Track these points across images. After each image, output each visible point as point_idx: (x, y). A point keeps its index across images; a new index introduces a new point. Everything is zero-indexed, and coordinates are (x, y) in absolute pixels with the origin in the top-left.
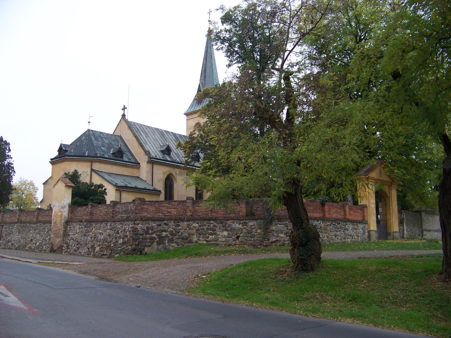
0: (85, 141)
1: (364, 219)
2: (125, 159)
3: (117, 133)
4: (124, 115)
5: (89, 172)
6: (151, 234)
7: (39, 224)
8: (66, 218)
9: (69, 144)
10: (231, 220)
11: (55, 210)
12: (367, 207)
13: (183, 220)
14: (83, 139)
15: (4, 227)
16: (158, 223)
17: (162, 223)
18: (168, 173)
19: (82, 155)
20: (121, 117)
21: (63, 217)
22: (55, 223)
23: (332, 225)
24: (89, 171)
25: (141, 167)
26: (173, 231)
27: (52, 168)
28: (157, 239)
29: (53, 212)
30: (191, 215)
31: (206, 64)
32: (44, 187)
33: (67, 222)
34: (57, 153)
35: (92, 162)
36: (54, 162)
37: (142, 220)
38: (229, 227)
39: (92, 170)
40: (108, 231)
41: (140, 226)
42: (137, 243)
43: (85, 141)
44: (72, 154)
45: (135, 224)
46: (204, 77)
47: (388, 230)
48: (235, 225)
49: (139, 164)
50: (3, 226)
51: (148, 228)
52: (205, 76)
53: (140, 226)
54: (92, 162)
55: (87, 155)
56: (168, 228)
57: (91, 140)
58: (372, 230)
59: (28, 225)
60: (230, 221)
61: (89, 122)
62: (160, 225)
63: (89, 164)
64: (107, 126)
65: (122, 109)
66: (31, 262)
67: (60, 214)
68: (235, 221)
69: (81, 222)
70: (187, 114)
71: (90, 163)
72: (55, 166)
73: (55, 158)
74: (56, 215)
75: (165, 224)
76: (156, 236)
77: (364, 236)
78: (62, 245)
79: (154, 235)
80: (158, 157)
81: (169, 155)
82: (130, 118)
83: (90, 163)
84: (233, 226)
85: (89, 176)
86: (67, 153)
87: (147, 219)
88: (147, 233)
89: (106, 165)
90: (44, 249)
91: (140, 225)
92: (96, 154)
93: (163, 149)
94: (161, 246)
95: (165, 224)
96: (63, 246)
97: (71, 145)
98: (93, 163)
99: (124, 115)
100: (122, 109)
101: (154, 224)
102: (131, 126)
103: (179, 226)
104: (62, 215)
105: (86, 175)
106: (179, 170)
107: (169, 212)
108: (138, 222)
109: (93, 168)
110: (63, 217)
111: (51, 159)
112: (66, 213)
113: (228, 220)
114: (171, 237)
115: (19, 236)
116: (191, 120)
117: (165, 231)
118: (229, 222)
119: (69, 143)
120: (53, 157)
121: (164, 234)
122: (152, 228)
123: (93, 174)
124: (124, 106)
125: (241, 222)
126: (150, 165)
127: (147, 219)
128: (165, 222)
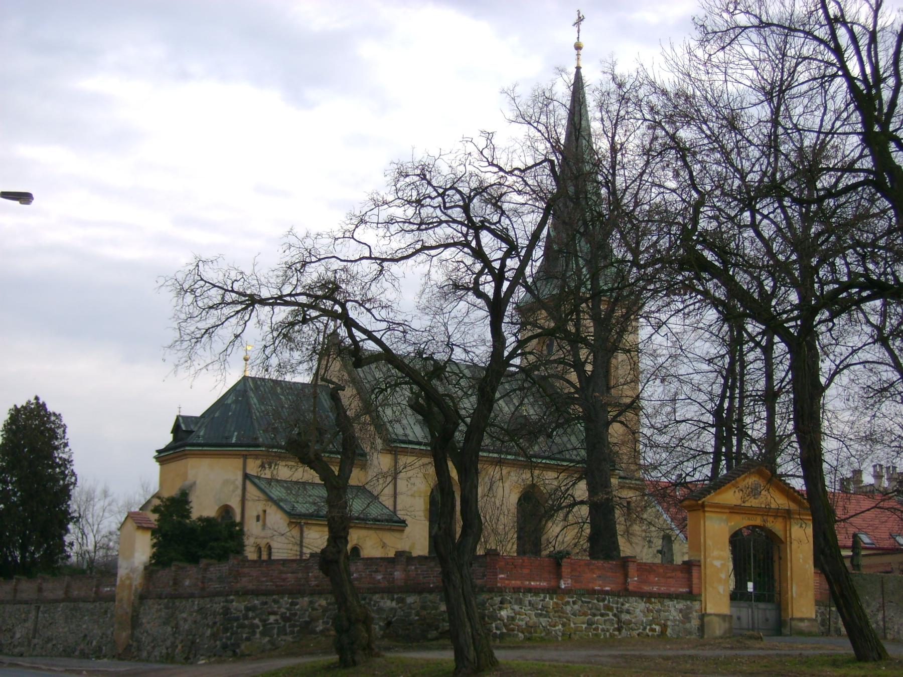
0: (233, 406)
1: (691, 592)
7: (97, 604)
8: (139, 590)
9: (198, 414)
10: (378, 593)
11: (122, 572)
12: (700, 566)
13: (302, 593)
14: (229, 401)
15: (41, 609)
16: (264, 599)
17: (269, 599)
19: (224, 442)
21: (134, 587)
22: (121, 600)
23: (580, 603)
29: (118, 579)
30: (317, 586)
33: (143, 597)
34: (169, 438)
35: (245, 457)
37: (237, 593)
38: (374, 606)
39: (246, 476)
41: (238, 606)
43: (233, 406)
44: (201, 441)
45: (227, 601)
47: (783, 614)
48: (385, 603)
51: (248, 609)
53: (238, 606)
55: (234, 441)
56: (279, 608)
57: (248, 404)
58: (710, 615)
60: (377, 596)
62: (266, 603)
63: (239, 462)
67: (128, 582)
68: (385, 595)
69: (160, 598)
71: (241, 461)
72: (173, 466)
73: (167, 449)
77: (688, 625)
79: (257, 621)
80: (411, 437)
83: (241, 461)
84: (382, 604)
85: (239, 492)
86: (192, 439)
87: (246, 593)
88: (246, 617)
90: (104, 651)
91: (234, 603)
92: (257, 438)
94: (267, 639)
97: (203, 416)
101: (256, 602)
103: (297, 604)
104: (131, 585)
105: (231, 488)
107: (284, 580)
108: (232, 597)
110: (134, 587)
111: (159, 451)
112: (138, 580)
113: (376, 593)
114: (282, 623)
115: (66, 629)
117: (274, 613)
118: (376, 597)
119: (198, 413)
120: (162, 447)
121: (272, 618)
122: (253, 609)
125: (396, 596)
127: (246, 593)
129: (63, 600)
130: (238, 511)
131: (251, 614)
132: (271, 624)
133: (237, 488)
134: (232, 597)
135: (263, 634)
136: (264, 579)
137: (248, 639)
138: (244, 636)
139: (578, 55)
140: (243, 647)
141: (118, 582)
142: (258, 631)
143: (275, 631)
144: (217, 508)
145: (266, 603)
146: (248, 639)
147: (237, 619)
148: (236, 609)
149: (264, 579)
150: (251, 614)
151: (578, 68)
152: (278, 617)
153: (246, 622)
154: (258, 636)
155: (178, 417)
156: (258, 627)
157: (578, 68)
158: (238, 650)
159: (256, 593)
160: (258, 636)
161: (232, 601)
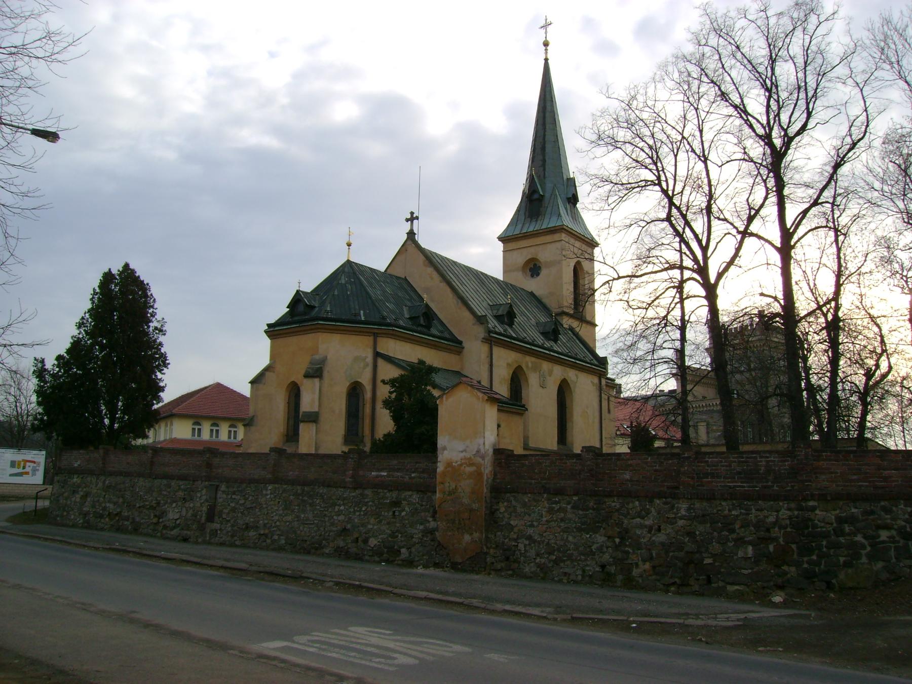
2: (434, 331)
3: (398, 272)
4: (411, 234)
5: (370, 359)
6: (849, 534)
18: (515, 366)
20: (405, 237)
24: (369, 355)
25: (465, 350)
26: (905, 526)
27: (271, 347)
28: (869, 548)
31: (544, 135)
32: (252, 388)
33: (497, 491)
34: (281, 310)
35: (376, 335)
36: (274, 331)
39: (377, 355)
40: (681, 523)
41: (824, 516)
42: (814, 557)
45: (800, 509)
46: (541, 163)
49: (460, 343)
50: (218, 486)
51: (840, 520)
52: (544, 161)
54: (376, 335)
59: (322, 490)
61: (349, 245)
62: (872, 512)
63: (369, 340)
64: (378, 256)
65: (407, 220)
66: (528, 615)
70: (503, 239)
71: (371, 338)
72: (280, 341)
74: (453, 470)
75: (884, 509)
76: (863, 541)
78: (485, 549)
79: (859, 538)
81: (511, 324)
82: (424, 241)
83: (371, 338)
86: (314, 313)
88: (839, 532)
89: (403, 343)
91: (817, 512)
93: (500, 313)
94: (880, 565)
95: (884, 509)
96: (486, 553)
98: (379, 339)
99: (411, 234)
100: (407, 220)
101: (853, 510)
102: (431, 260)
105: (362, 365)
106: (533, 359)
108: (811, 503)
109: (379, 350)
111: (269, 325)
114: (902, 542)
116: (515, 252)
117: (887, 527)
120: (273, 321)
121: (884, 535)
122: (852, 520)
123: (380, 361)
124: (412, 213)
126: (485, 348)
128: (882, 503)
129: (271, 482)
130: (368, 388)
131: (847, 528)
132: (884, 542)
133: (367, 365)
134: (811, 503)
135: (872, 557)
136: (855, 477)
137: (847, 565)
138: (842, 559)
139: (546, 50)
140: (842, 576)
141: (440, 468)
142: (863, 552)
143: (892, 553)
144: (348, 384)
145: (872, 512)
146: (847, 565)
147: (826, 535)
148: (823, 521)
149: (855, 477)
150: (847, 528)
151: (546, 60)
152: (894, 533)
153: (842, 539)
154: (864, 560)
155: (298, 291)
156: (863, 547)
157: (546, 60)
158: (834, 581)
159: (853, 498)
160: (864, 560)
161: (813, 509)
